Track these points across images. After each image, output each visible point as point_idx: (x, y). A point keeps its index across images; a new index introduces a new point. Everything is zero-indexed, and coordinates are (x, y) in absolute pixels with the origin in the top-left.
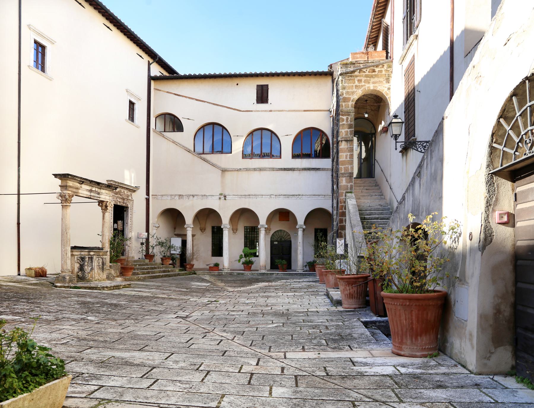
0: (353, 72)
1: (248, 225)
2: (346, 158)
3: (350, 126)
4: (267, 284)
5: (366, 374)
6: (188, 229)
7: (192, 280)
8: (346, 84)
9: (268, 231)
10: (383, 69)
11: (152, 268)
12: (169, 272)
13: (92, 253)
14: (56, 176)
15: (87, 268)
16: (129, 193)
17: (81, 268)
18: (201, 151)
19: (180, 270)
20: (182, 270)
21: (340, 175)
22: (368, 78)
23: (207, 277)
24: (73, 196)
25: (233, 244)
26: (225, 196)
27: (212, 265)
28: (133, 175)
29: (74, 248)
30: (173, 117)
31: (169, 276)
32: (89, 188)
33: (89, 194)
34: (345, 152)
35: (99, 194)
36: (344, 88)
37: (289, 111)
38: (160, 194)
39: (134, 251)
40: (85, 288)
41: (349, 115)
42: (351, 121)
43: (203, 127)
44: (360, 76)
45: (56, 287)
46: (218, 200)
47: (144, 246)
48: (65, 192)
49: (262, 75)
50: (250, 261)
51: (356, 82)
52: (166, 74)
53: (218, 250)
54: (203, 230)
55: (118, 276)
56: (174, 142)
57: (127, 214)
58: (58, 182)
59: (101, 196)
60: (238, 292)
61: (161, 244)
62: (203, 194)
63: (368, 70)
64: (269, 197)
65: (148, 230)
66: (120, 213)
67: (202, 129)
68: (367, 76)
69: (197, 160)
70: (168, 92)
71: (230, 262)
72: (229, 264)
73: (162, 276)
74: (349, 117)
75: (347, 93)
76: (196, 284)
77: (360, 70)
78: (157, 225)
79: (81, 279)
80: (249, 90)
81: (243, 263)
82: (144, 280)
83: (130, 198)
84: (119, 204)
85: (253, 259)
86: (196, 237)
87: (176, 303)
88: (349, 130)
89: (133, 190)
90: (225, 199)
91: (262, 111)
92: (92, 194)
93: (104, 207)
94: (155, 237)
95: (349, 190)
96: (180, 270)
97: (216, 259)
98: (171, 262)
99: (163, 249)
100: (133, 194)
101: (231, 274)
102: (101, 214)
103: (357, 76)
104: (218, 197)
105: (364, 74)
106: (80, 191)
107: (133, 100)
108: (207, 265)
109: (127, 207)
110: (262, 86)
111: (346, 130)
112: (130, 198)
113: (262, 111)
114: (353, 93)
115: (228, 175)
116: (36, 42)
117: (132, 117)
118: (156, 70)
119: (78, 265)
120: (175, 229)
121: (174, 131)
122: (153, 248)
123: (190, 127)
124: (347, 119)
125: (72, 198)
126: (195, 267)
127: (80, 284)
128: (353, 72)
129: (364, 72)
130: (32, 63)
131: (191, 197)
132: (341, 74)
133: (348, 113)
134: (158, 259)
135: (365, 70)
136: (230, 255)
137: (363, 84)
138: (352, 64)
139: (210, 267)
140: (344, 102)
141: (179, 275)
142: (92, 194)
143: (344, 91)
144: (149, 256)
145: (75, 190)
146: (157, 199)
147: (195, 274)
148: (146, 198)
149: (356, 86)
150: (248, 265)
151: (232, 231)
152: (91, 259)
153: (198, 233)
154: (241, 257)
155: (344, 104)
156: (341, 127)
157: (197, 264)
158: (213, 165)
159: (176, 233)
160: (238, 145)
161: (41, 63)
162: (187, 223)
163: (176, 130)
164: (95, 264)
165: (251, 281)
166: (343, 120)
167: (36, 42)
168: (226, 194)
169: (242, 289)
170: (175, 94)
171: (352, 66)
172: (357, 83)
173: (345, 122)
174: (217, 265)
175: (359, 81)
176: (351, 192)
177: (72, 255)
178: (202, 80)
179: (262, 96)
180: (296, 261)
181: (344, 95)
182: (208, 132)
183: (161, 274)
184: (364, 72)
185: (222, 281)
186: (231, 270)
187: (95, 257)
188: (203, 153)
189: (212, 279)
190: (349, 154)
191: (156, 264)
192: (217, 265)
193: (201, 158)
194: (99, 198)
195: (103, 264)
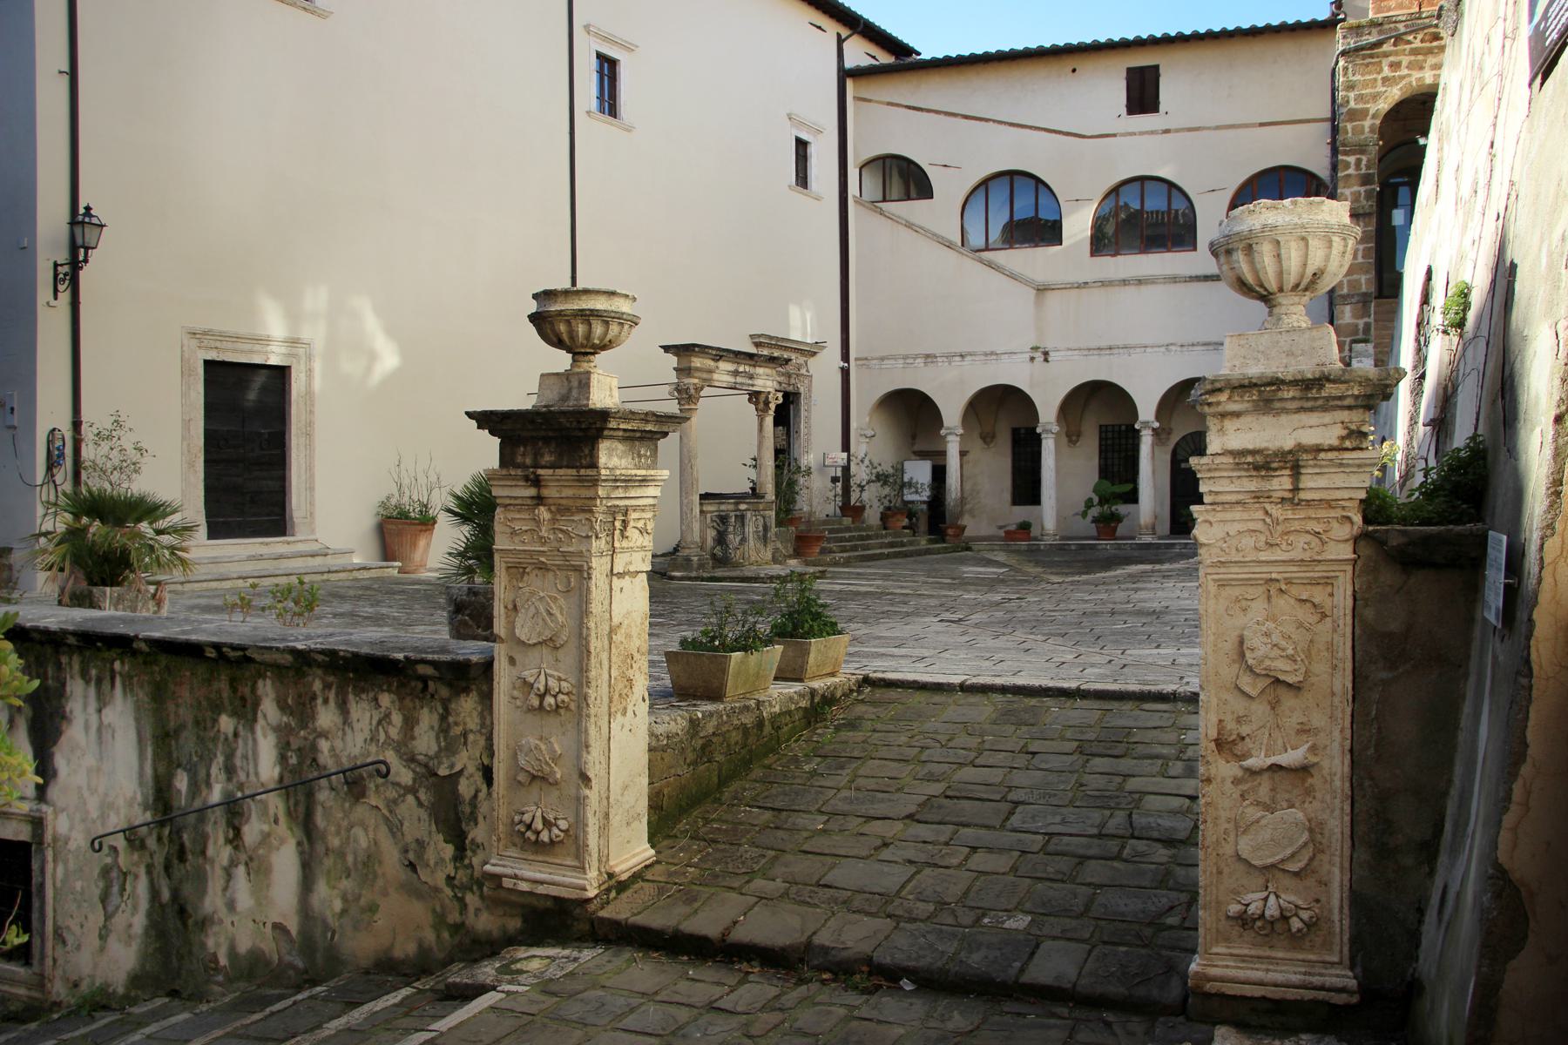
0: (1379, 44)
1: (1108, 420)
3: (1366, 180)
4: (1148, 567)
6: (950, 438)
7: (963, 561)
8: (1358, 77)
9: (1163, 436)
11: (862, 538)
12: (903, 544)
13: (743, 507)
14: (667, 349)
15: (733, 539)
16: (801, 360)
17: (721, 539)
18: (981, 243)
19: (931, 541)
20: (937, 542)
21: (1336, 301)
22: (1420, 57)
23: (1001, 557)
25: (1066, 473)
26: (1046, 354)
27: (1013, 528)
28: (808, 317)
29: (705, 497)
30: (905, 164)
31: (906, 555)
32: (730, 367)
33: (731, 379)
35: (751, 377)
36: (1351, 87)
37: (1218, 128)
38: (878, 355)
39: (817, 497)
40: (732, 579)
41: (1362, 152)
42: (1368, 167)
43: (985, 184)
44: (1396, 53)
45: (672, 578)
46: (1029, 364)
47: (839, 484)
48: (686, 381)
49: (1139, 44)
50: (1113, 514)
51: (1386, 69)
52: (885, 59)
53: (1027, 488)
54: (988, 438)
55: (790, 557)
56: (909, 225)
57: (798, 411)
58: (672, 360)
60: (1072, 583)
61: (882, 478)
62: (988, 350)
63: (1420, 37)
65: (846, 446)
66: (786, 412)
67: (982, 189)
68: (1415, 52)
69: (969, 265)
70: (889, 104)
71: (1060, 519)
72: (1058, 521)
73: (888, 556)
74: (1364, 159)
75: (1360, 98)
76: (970, 571)
77: (1398, 39)
78: (870, 433)
79: (721, 561)
80: (1109, 86)
81: (1095, 520)
82: (847, 563)
83: (803, 371)
85: (1122, 509)
86: (970, 457)
87: (933, 602)
88: (1362, 189)
89: (810, 352)
90: (1046, 360)
91: (1142, 133)
92: (739, 380)
93: (761, 406)
94: (867, 462)
95: (1361, 336)
96: (931, 541)
97: (1022, 513)
98: (906, 522)
99: (887, 490)
100: (811, 361)
101: (1061, 549)
103: (1386, 55)
104: (1027, 356)
107: (804, 136)
108: (1001, 527)
110: (1142, 70)
111: (1356, 188)
112: (803, 371)
113: (1142, 133)
114: (1375, 97)
115: (1051, 297)
116: (600, 56)
117: (802, 179)
118: (859, 53)
119: (714, 533)
120: (914, 437)
121: (909, 199)
122: (862, 488)
123: (950, 187)
124: (1358, 162)
126: (967, 533)
127: (719, 573)
128: (1379, 44)
129: (1409, 42)
130: (594, 104)
132: (1343, 53)
133: (1361, 149)
134: (872, 516)
135: (1410, 38)
136: (1060, 501)
137: (1405, 72)
138: (1374, 24)
139: (1007, 533)
140: (1351, 120)
141: (928, 552)
142: (739, 380)
143: (1352, 95)
144: (851, 510)
145: (705, 376)
146: (868, 367)
147: (968, 549)
148: (842, 369)
149: (1385, 80)
150: (1108, 524)
151: (1065, 440)
152: (741, 518)
153: (977, 448)
154: (1089, 504)
155: (1349, 126)
156: (1341, 184)
157: (973, 526)
158: (1012, 276)
159: (916, 448)
160: (1078, 225)
161: (609, 103)
162: (946, 423)
164: (750, 529)
165: (1109, 563)
166: (1347, 166)
167: (600, 56)
168: (1049, 346)
169: (1084, 577)
170: (909, 107)
171: (1374, 31)
172: (1386, 72)
173: (1351, 171)
174: (1025, 527)
175: (1395, 66)
176: (1366, 341)
177: (702, 512)
178: (979, 68)
179: (1143, 95)
180: (86, 620)
181: (1352, 104)
182: (999, 195)
183: (886, 551)
184: (1409, 42)
185: (1037, 563)
186: (1062, 538)
187: (749, 514)
188: (987, 249)
189: (1013, 561)
191: (869, 528)
192: (1025, 527)
193: (981, 261)
195: (766, 528)
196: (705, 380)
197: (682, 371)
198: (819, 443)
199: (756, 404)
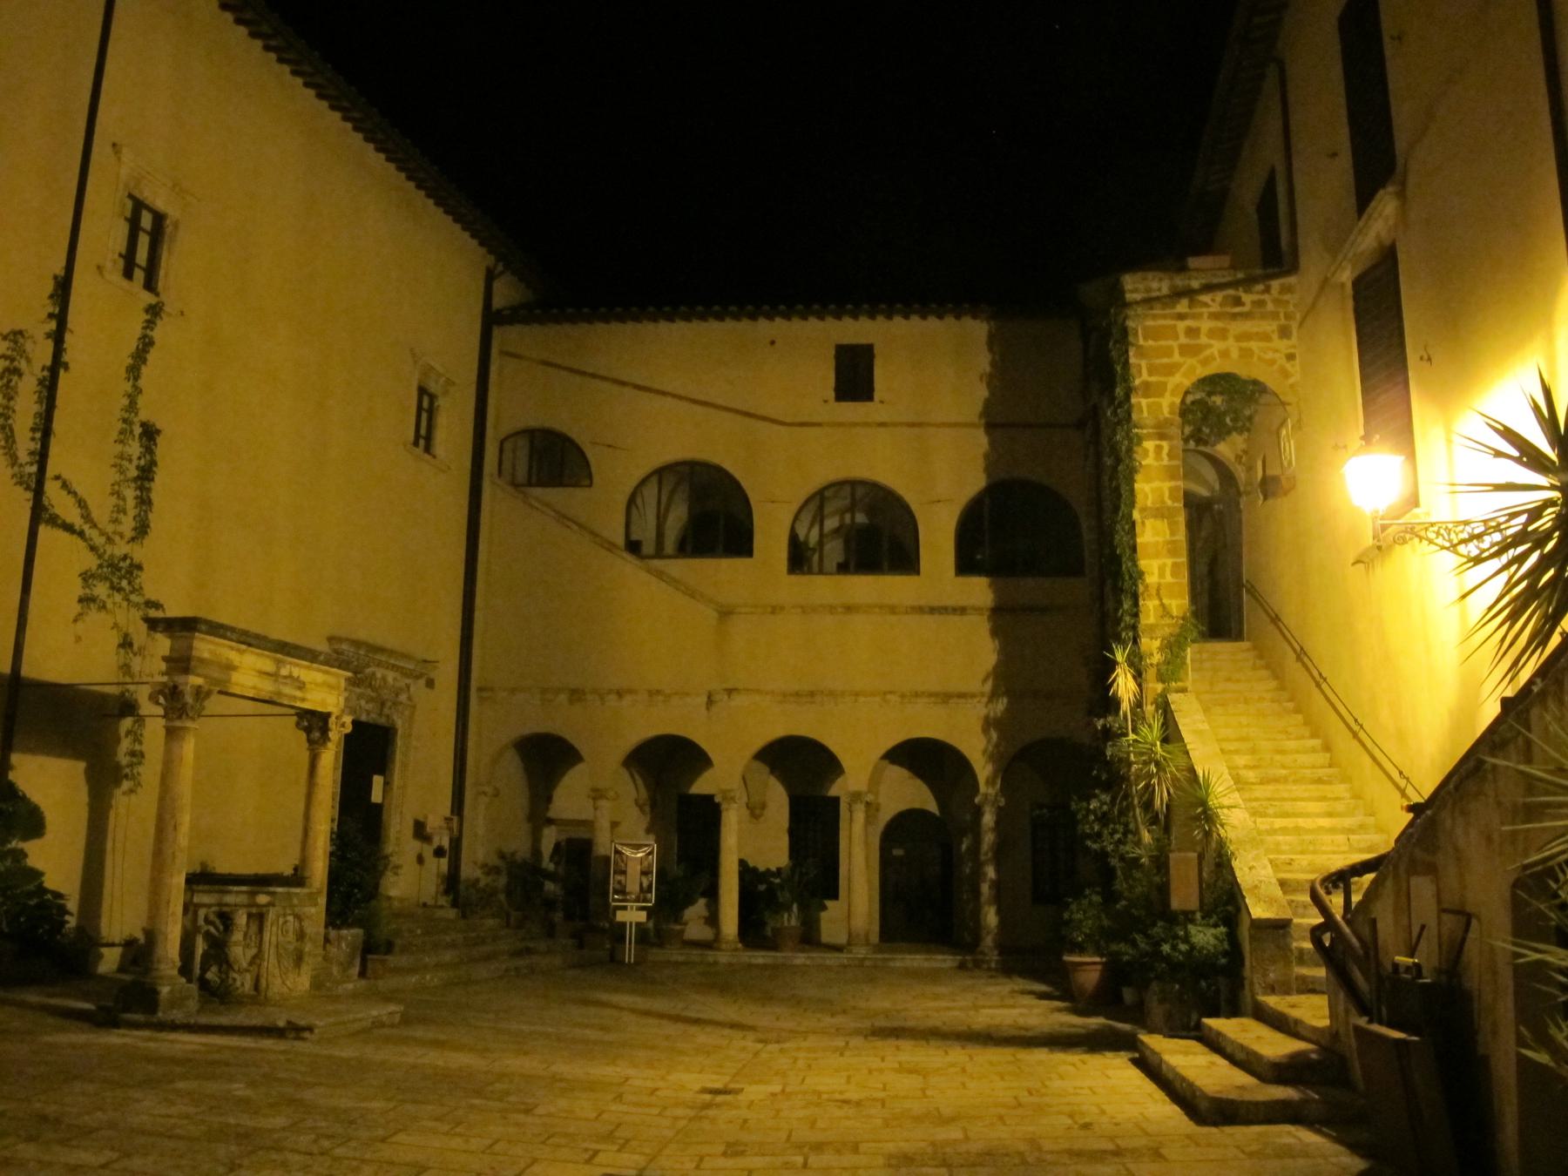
2: (1162, 575)
3: (1171, 474)
5: (1108, 589)
10: (1266, 297)
13: (262, 899)
24: (209, 694)
34: (1157, 556)
59: (309, 696)
64: (878, 699)
66: (369, 749)
83: (403, 697)
102: (305, 756)
105: (1205, 310)
112: (403, 697)
117: (424, 439)
125: (206, 703)
129: (1206, 305)
131: (613, 697)
140: (1146, 396)
152: (259, 918)
155: (1144, 402)
163: (689, 548)
172: (1183, 340)
177: (188, 907)
180: (616, 990)
184: (1206, 305)
190: (1169, 562)
196: (217, 682)
197: (180, 663)
198: (415, 789)
199: (308, 730)
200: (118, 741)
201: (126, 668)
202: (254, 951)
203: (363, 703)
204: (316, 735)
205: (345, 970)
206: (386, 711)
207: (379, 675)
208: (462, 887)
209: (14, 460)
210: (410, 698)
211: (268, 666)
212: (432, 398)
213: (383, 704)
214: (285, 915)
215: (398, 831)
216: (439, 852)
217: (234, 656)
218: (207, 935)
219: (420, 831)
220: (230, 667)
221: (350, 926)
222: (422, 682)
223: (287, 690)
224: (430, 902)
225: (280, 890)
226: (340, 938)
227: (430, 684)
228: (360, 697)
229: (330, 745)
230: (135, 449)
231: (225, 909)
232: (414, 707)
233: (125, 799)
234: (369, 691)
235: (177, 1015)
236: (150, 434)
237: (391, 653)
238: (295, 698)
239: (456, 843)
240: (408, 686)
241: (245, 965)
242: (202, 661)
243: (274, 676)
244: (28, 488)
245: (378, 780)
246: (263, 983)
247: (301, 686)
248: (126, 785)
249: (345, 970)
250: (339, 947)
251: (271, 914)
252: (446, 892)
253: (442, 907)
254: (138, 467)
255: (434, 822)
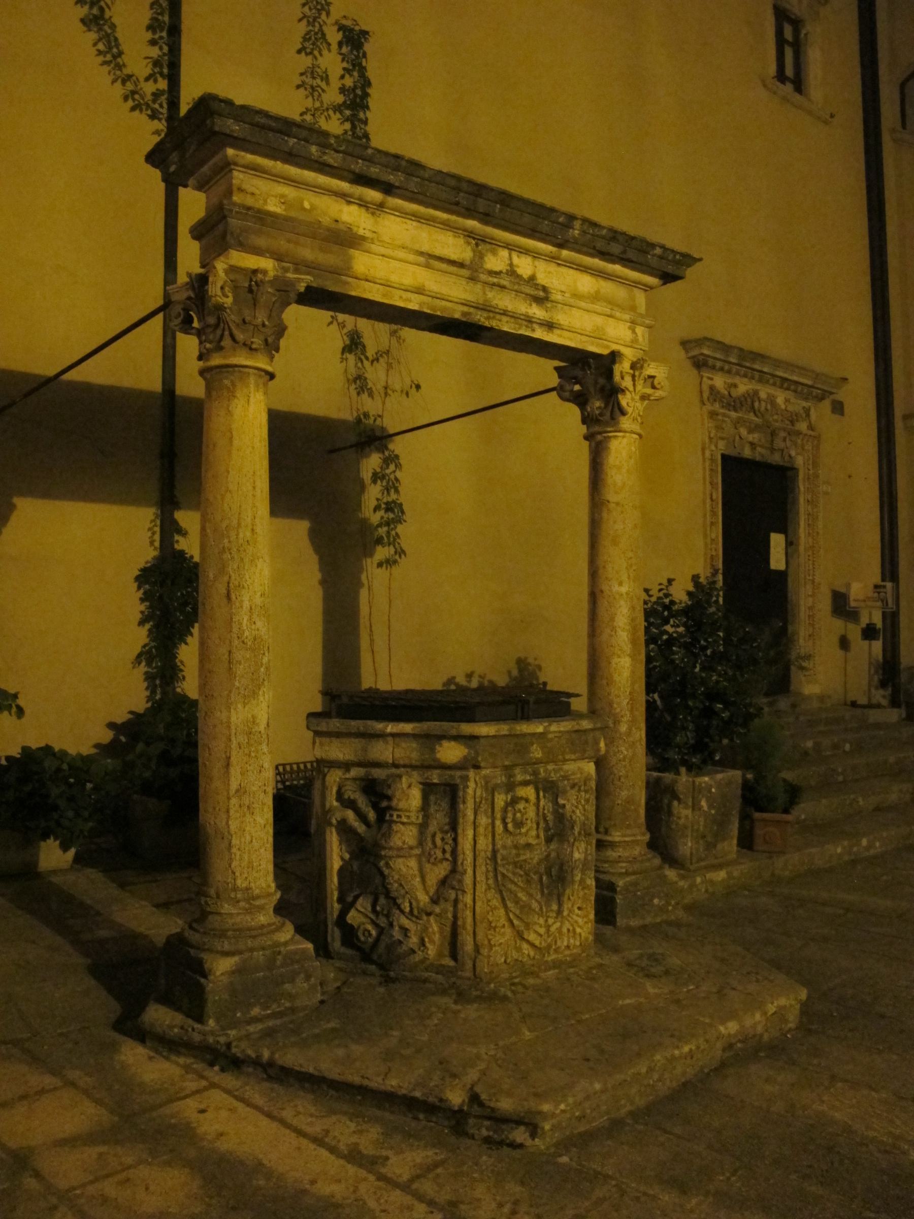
13: (451, 752)
16: (798, 405)
57: (795, 502)
59: (561, 318)
84: (747, 453)
106: (361, 262)
109: (794, 469)
112: (803, 426)
152: (446, 793)
194: (550, 326)
200: (363, 487)
201: (360, 383)
202: (442, 870)
203: (743, 432)
204: (597, 404)
205: (710, 846)
206: (779, 443)
207: (763, 395)
208: (904, 677)
209: (111, 51)
210: (811, 427)
211: (453, 247)
212: (797, 24)
213: (773, 434)
214: (510, 787)
215: (810, 603)
216: (869, 633)
217: (352, 216)
218: (344, 829)
219: (841, 605)
220: (345, 239)
221: (724, 764)
222: (827, 404)
223: (505, 301)
224: (863, 701)
225: (484, 729)
226: (696, 791)
227: (838, 408)
228: (737, 423)
229: (625, 423)
230: (332, 62)
231: (378, 773)
232: (818, 438)
233: (382, 573)
234: (752, 416)
235: (237, 1040)
236: (354, 39)
237: (777, 363)
238: (529, 321)
239: (892, 619)
240: (807, 411)
241: (423, 898)
242: (262, 218)
243: (471, 270)
244: (154, 116)
245: (777, 541)
246: (467, 943)
247: (542, 297)
248: (382, 553)
249: (710, 846)
250: (695, 807)
251: (473, 789)
252: (883, 684)
253: (879, 706)
254: (343, 90)
255: (858, 591)
